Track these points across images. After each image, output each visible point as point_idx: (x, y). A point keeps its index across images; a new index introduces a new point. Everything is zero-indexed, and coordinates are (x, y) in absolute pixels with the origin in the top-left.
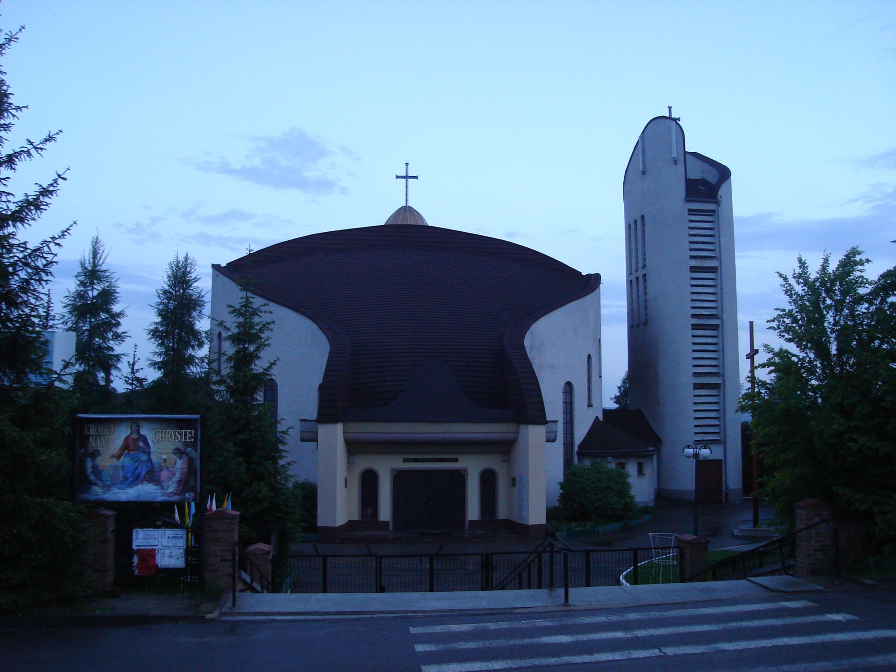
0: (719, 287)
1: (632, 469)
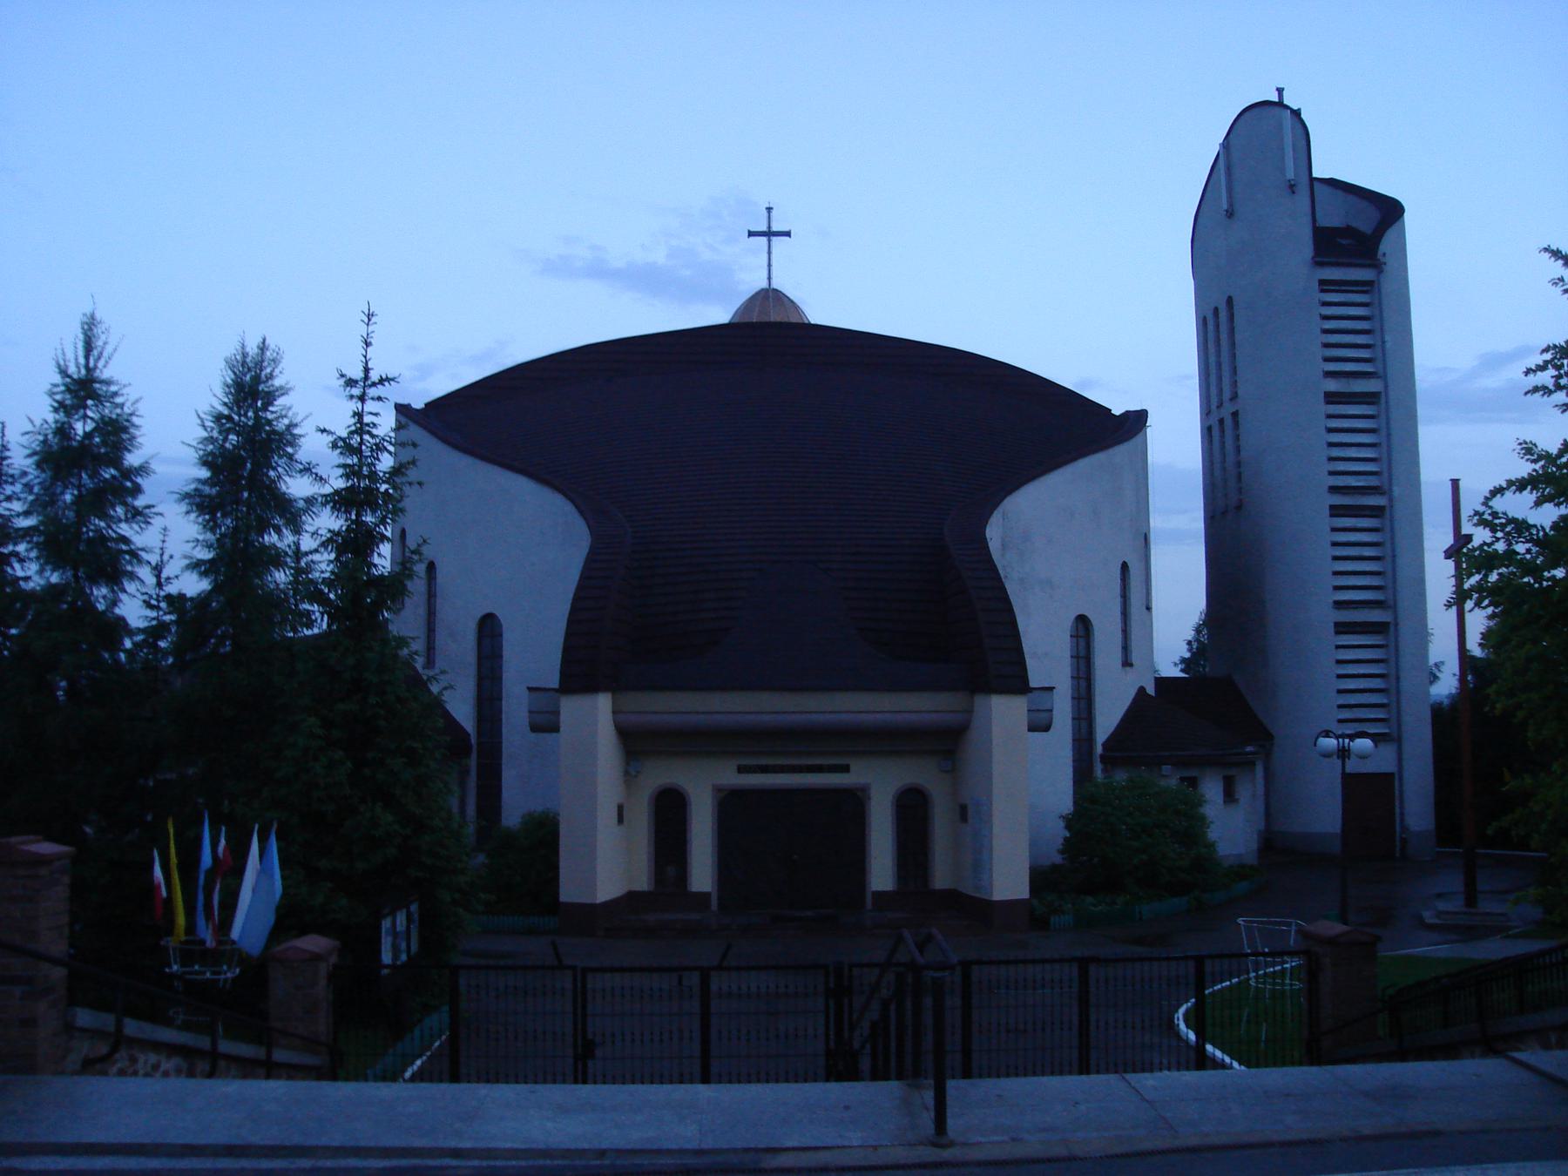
0: (1383, 432)
1: (1212, 789)
